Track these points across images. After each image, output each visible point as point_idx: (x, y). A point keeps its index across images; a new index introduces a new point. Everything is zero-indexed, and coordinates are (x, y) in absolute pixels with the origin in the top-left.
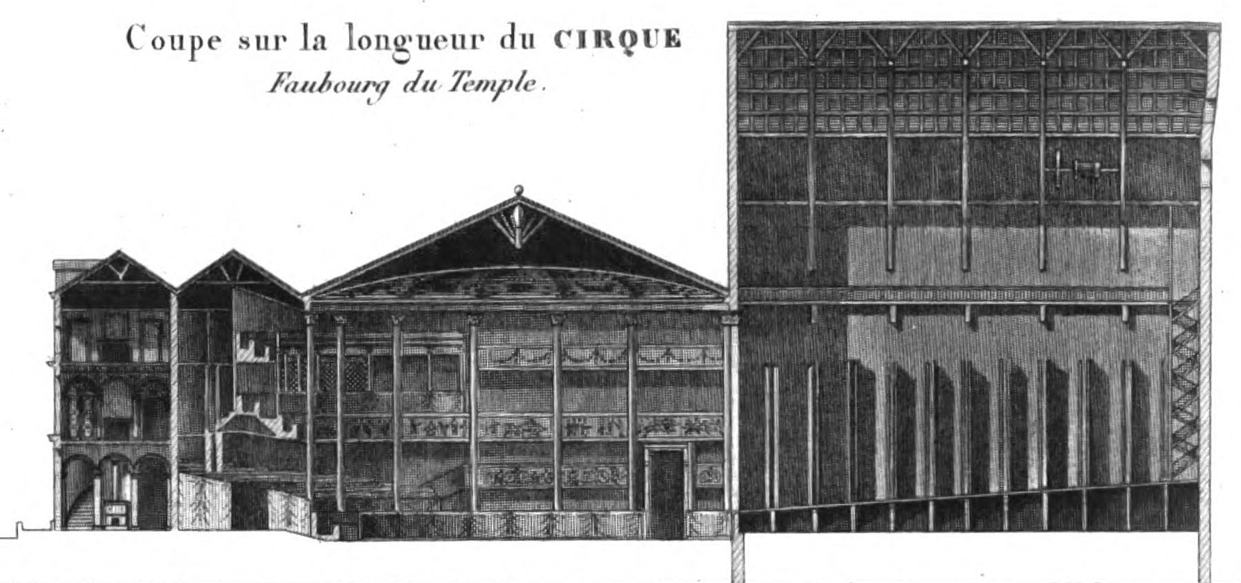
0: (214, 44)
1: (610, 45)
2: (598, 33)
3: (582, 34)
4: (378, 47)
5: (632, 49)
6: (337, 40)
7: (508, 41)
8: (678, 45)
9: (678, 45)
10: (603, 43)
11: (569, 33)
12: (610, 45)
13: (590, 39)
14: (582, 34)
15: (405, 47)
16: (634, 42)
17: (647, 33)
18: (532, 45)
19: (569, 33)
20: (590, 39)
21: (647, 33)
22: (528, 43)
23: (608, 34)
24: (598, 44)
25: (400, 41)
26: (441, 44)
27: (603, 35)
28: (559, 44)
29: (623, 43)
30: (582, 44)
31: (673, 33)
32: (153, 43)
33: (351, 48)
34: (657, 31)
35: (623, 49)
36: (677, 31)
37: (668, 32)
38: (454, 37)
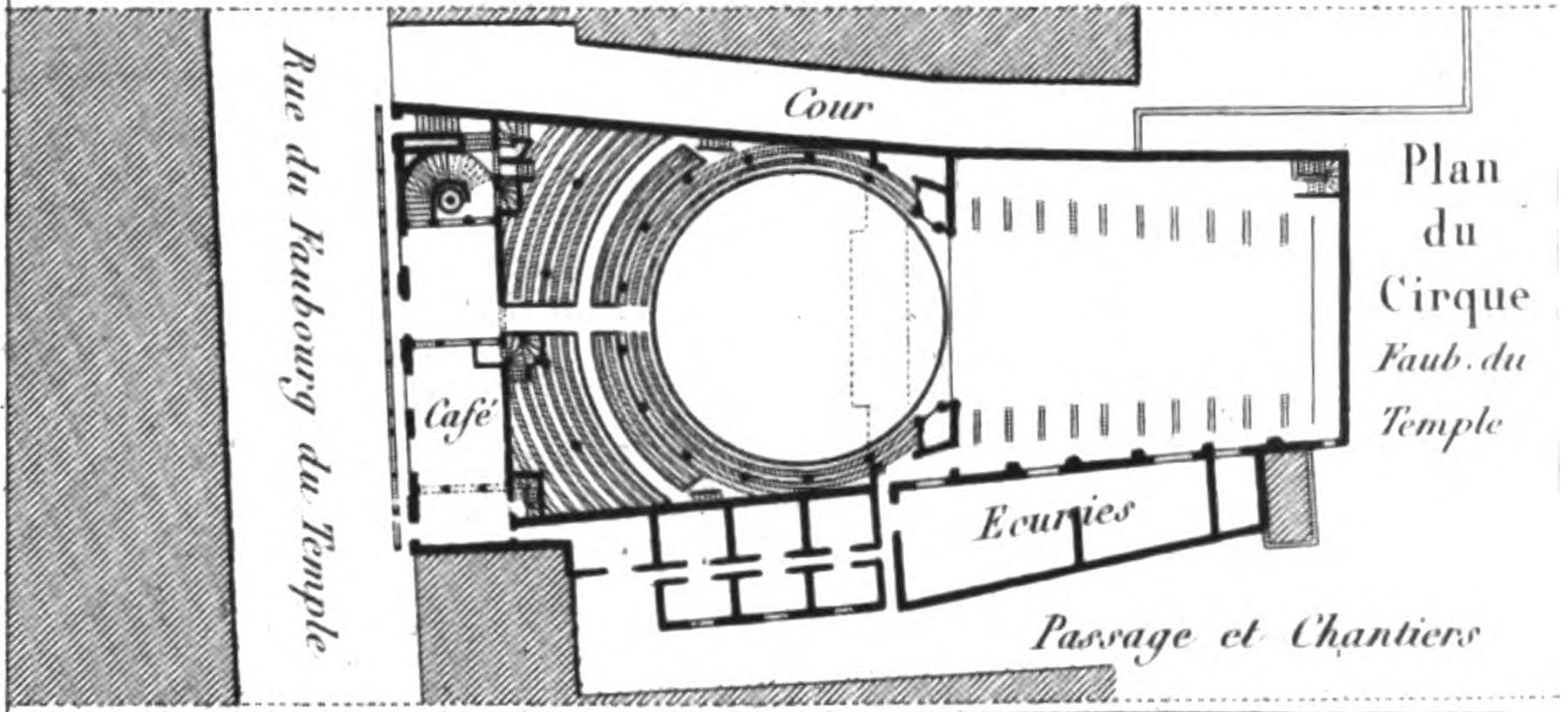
4: (1501, 293)
18: (1495, 178)
32: (1428, 241)
38: (1500, 306)
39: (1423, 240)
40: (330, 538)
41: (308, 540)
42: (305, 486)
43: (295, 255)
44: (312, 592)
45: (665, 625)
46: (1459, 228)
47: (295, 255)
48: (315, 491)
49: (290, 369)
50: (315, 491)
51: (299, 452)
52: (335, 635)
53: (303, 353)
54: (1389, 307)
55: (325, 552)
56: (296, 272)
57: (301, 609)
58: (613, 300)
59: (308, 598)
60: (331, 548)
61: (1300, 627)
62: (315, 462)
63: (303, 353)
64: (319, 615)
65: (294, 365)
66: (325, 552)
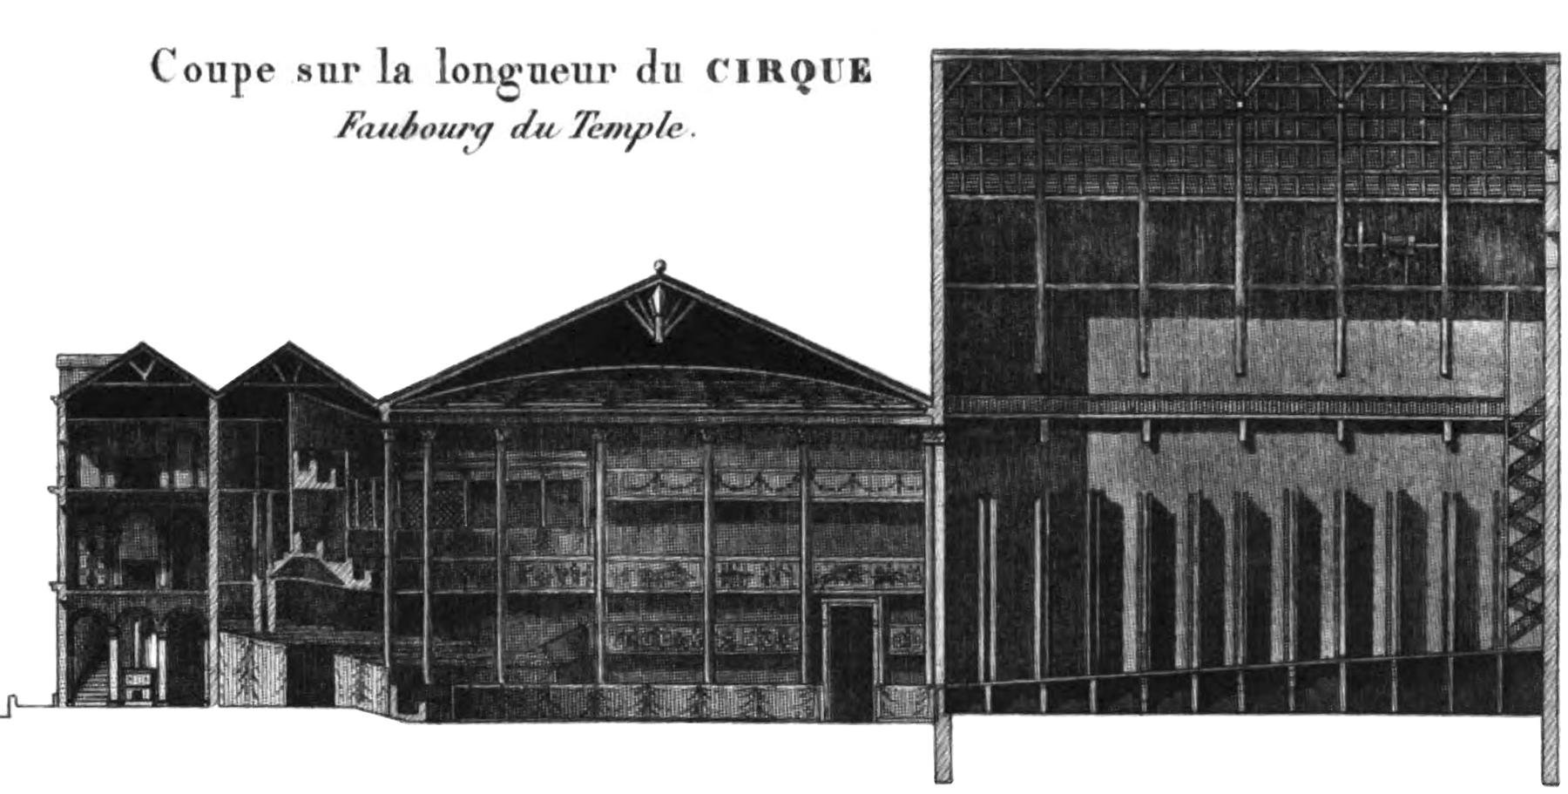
0: (266, 75)
1: (779, 78)
2: (763, 63)
3: (743, 65)
5: (808, 84)
6: (425, 69)
7: (647, 73)
8: (868, 79)
9: (868, 79)
10: (771, 75)
11: (726, 63)
12: (779, 78)
13: (754, 70)
14: (743, 65)
15: (513, 79)
16: (810, 75)
17: (827, 62)
19: (726, 63)
20: (754, 70)
21: (827, 62)
22: (328, 76)
23: (777, 64)
24: (764, 78)
25: (507, 73)
26: (560, 77)
27: (770, 65)
28: (713, 76)
29: (795, 76)
30: (743, 76)
31: (861, 63)
33: (443, 80)
34: (840, 61)
35: (796, 85)
36: (866, 60)
37: (855, 62)
38: (577, 67)
39: (152, 74)
40: (589, 113)
41: (590, 134)
42: (547, 135)
43: (368, 135)
44: (632, 133)
45: (9, 716)
46: (668, 66)
47: (368, 135)
48: (552, 126)
49: (456, 144)
50: (552, 126)
51: (365, 139)
52: (668, 114)
53: (446, 132)
54: (158, 76)
55: (600, 120)
56: (381, 134)
57: (647, 144)
58: (114, 696)
59: (637, 136)
60: (597, 113)
61: (156, 57)
62: (527, 126)
63: (446, 132)
64: (651, 126)
65: (454, 141)
66: (600, 120)
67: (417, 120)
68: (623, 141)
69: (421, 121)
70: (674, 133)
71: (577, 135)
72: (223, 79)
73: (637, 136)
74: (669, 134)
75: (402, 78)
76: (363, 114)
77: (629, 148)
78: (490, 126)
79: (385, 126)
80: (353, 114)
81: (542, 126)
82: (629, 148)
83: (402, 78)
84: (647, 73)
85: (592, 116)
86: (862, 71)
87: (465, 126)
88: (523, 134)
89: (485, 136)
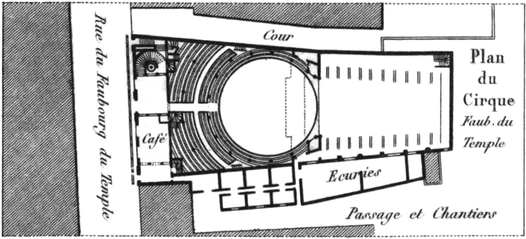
0: (511, 103)
7: (482, 80)
22: (500, 58)
47: (99, 85)
48: (106, 164)
50: (106, 164)
53: (102, 118)
55: (109, 185)
59: (103, 200)
62: (105, 154)
63: (102, 118)
64: (107, 206)
67: (106, 105)
68: (100, 194)
69: (105, 107)
70: (98, 37)
71: (103, 176)
72: (490, 78)
73: (103, 200)
74: (104, 213)
75: (490, 61)
76: (108, 84)
77: (98, 197)
78: (104, 137)
79: (103, 93)
80: (107, 79)
81: (106, 160)
82: (98, 197)
83: (490, 61)
84: (482, 80)
85: (110, 182)
86: (334, 176)
87: (104, 126)
88: (101, 153)
89: (99, 135)
